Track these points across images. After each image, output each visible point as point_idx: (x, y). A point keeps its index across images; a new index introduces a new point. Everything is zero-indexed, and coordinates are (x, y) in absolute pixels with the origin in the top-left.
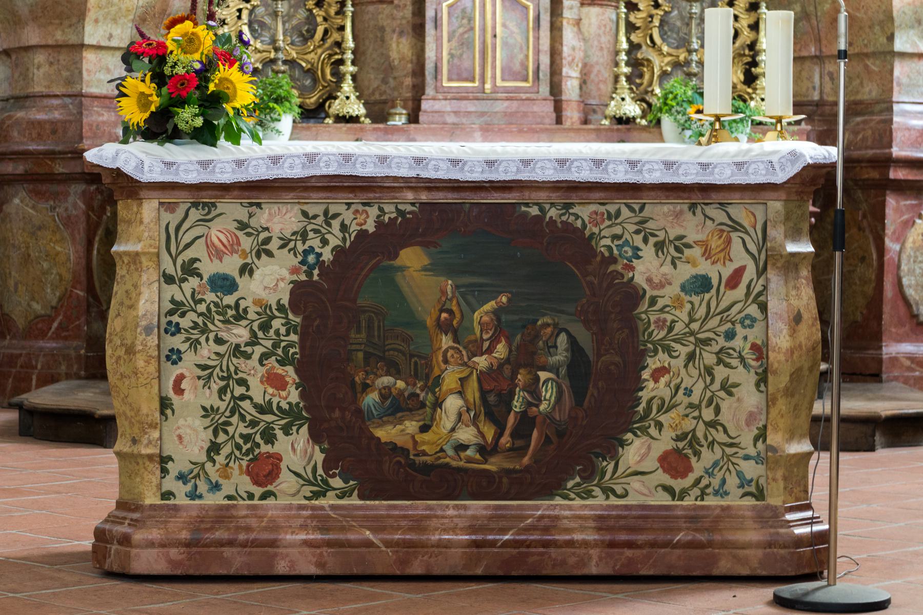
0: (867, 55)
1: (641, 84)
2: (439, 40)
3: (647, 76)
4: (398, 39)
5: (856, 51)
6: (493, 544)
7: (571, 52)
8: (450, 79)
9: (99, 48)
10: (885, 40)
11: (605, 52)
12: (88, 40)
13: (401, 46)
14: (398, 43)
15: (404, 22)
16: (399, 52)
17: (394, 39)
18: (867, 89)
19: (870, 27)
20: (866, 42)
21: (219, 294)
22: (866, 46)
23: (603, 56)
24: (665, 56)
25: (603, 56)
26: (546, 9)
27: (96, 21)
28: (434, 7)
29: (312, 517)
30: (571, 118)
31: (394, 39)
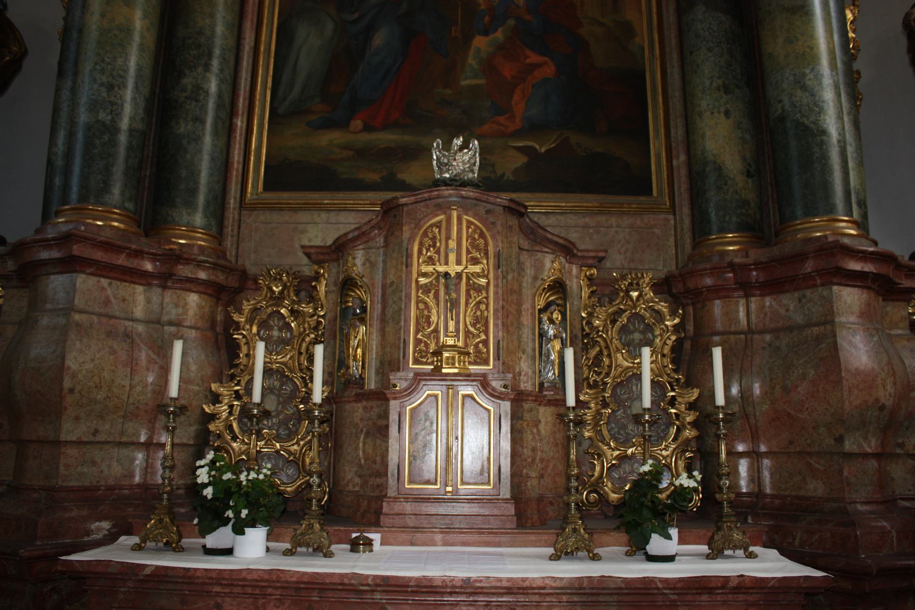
0: (810, 454)
1: (593, 476)
2: (400, 440)
3: (598, 468)
4: (364, 439)
5: (798, 449)
6: (448, 238)
7: (530, 453)
8: (410, 482)
9: (79, 443)
10: (832, 442)
11: (560, 447)
12: (63, 437)
13: (367, 446)
14: (364, 443)
15: (370, 423)
16: (364, 452)
17: (362, 439)
18: (812, 487)
19: (814, 428)
20: (809, 441)
21: (401, 385)
22: (809, 445)
23: (558, 451)
24: (613, 450)
25: (558, 451)
26: (506, 413)
27: (77, 418)
28: (398, 410)
29: (451, 311)
30: (532, 519)
31: (362, 439)
